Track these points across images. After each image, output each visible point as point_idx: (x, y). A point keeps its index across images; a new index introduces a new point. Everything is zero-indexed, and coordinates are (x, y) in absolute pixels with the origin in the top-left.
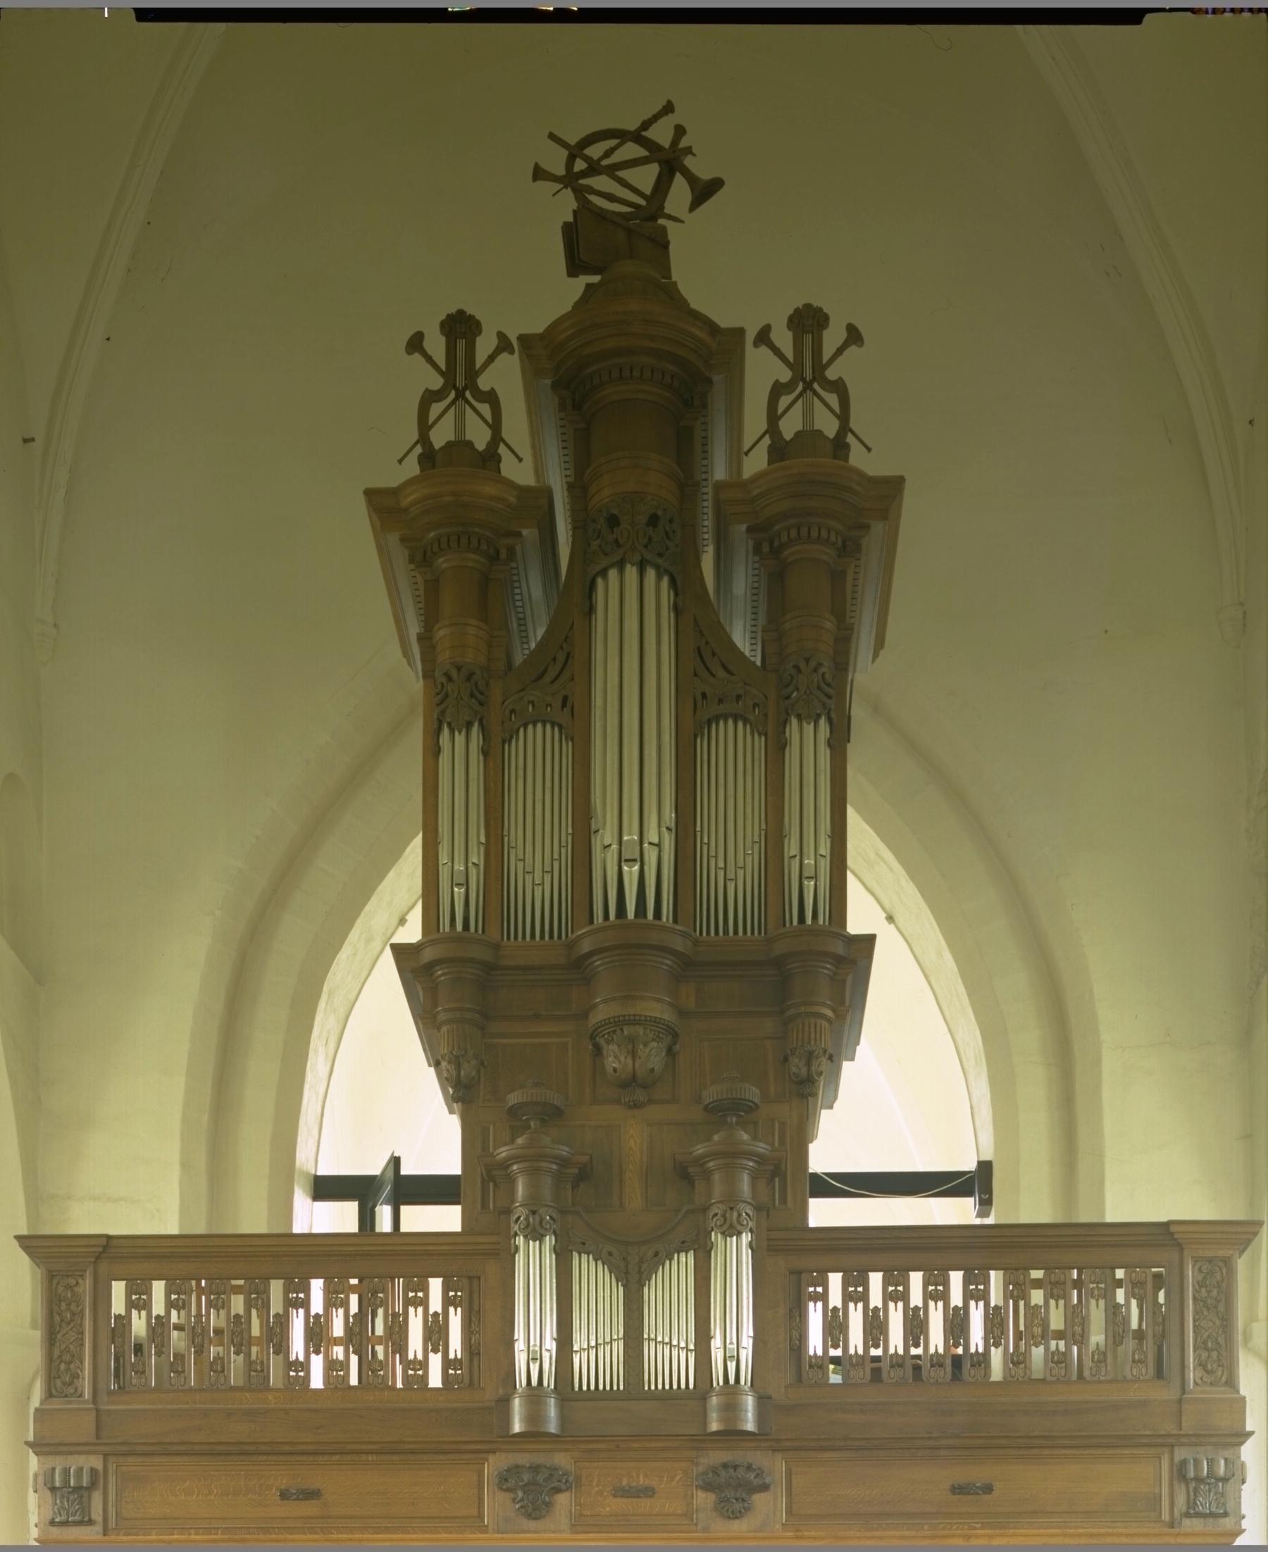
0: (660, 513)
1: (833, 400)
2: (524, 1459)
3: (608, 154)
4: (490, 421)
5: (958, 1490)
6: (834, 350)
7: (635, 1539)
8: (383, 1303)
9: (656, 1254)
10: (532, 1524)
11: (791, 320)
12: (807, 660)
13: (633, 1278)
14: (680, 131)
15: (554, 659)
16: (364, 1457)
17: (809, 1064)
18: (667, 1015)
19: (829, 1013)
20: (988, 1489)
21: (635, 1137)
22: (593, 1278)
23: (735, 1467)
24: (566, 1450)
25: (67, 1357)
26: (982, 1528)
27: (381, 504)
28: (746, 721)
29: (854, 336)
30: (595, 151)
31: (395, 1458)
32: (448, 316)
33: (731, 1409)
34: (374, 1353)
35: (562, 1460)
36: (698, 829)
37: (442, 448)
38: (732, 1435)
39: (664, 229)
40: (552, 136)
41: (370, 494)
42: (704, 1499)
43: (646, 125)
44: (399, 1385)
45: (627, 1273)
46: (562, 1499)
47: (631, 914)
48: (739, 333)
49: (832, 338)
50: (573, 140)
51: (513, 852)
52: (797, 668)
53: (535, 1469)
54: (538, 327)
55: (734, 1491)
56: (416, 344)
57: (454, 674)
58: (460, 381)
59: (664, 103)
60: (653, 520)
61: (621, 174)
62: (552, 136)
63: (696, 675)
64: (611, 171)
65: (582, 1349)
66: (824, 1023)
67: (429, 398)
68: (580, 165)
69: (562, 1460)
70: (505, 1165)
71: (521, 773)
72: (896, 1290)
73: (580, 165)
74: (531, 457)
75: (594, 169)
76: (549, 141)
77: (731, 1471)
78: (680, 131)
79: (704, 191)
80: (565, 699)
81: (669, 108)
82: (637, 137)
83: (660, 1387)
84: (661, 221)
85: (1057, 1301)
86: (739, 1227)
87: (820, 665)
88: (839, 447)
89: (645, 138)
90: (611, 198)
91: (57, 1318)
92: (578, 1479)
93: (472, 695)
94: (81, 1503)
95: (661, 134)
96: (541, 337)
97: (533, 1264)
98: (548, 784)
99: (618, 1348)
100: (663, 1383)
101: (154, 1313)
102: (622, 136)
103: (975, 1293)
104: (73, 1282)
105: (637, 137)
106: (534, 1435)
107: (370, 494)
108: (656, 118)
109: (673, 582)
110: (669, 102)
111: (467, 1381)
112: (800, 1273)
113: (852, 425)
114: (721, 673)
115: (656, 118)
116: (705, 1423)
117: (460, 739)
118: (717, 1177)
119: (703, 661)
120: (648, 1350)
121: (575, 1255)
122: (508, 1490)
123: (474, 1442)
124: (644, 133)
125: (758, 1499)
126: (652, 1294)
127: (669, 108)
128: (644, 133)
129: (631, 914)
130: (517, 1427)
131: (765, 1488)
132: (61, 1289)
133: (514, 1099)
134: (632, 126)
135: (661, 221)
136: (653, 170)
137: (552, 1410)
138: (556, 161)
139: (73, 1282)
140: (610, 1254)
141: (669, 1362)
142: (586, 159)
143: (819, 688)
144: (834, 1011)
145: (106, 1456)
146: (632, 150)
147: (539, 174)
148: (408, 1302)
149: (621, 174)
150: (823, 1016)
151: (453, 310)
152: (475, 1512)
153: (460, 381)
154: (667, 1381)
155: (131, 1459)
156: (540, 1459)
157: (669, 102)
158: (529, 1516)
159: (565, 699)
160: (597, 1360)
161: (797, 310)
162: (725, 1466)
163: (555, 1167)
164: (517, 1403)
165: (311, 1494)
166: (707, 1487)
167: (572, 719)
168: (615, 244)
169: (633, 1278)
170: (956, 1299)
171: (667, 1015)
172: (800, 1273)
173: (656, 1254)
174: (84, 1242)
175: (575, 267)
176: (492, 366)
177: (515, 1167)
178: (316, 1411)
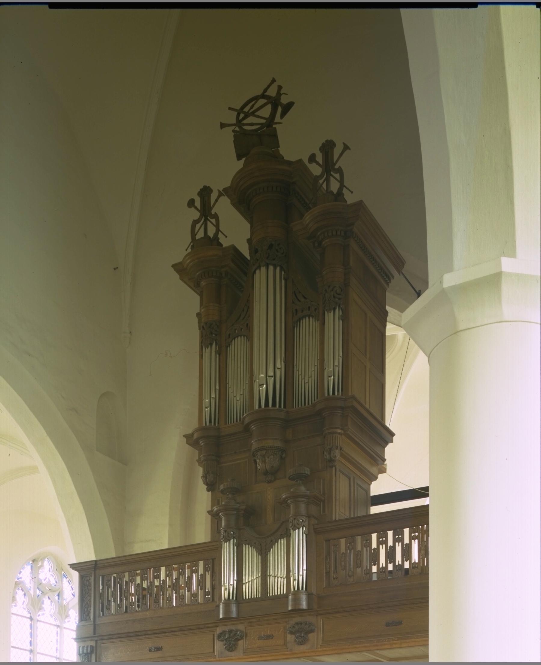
0: (273, 243)
1: (213, 221)
2: (227, 628)
3: (252, 108)
4: (215, 224)
5: (388, 625)
6: (339, 155)
7: (266, 656)
8: (147, 579)
9: (272, 541)
10: (232, 654)
11: (320, 149)
12: (329, 287)
13: (263, 554)
14: (280, 88)
15: (243, 310)
16: (176, 633)
17: (330, 454)
18: (278, 444)
19: (339, 431)
20: (400, 623)
21: (268, 494)
22: (251, 555)
23: (301, 624)
24: (242, 623)
25: (87, 606)
26: (398, 640)
27: (178, 268)
28: (313, 317)
29: (346, 148)
30: (246, 109)
31: (186, 632)
32: (201, 189)
33: (297, 600)
34: (132, 599)
35: (241, 627)
36: (295, 365)
37: (199, 239)
38: (297, 611)
39: (275, 129)
40: (230, 109)
41: (174, 266)
42: (290, 638)
43: (265, 90)
44: (174, 605)
45: (261, 550)
46: (241, 643)
47: (263, 406)
48: (300, 161)
49: (337, 152)
50: (238, 108)
51: (230, 389)
52: (326, 290)
53: (230, 631)
54: (228, 184)
55: (302, 633)
56: (191, 203)
57: (205, 326)
58: (206, 212)
59: (272, 79)
60: (271, 247)
61: (256, 114)
62: (230, 109)
63: (293, 303)
64: (253, 114)
65: (249, 581)
66: (339, 436)
67: (195, 222)
68: (242, 116)
69: (241, 627)
70: (285, 501)
71: (233, 358)
72: (415, 535)
73: (242, 116)
74: (235, 231)
75: (247, 116)
76: (230, 111)
77: (299, 625)
78: (280, 88)
79: (287, 108)
80: (247, 324)
81: (274, 81)
82: (263, 96)
83: (279, 593)
84: (274, 126)
85: (367, 548)
86: (298, 526)
87: (335, 287)
88: (340, 194)
89: (266, 95)
90: (252, 124)
91: (84, 592)
92: (246, 635)
93: (334, 297)
94: (88, 659)
95: (272, 92)
96: (230, 187)
97: (228, 551)
98: (242, 360)
99: (259, 581)
100: (274, 593)
101: (162, 579)
102: (256, 99)
103: (398, 539)
104: (88, 578)
105: (263, 96)
106: (227, 619)
107: (174, 266)
108: (269, 86)
109: (282, 269)
110: (273, 78)
111: (211, 599)
112: (329, 540)
113: (345, 184)
114: (303, 300)
115: (269, 86)
116: (288, 607)
117: (208, 350)
118: (292, 506)
119: (296, 296)
120: (269, 580)
121: (244, 546)
122: (221, 641)
123: (212, 623)
124: (265, 94)
125: (310, 636)
126: (271, 557)
127: (274, 81)
128: (265, 94)
129: (263, 406)
130: (221, 617)
131: (312, 631)
132: (85, 582)
133: (222, 487)
134: (260, 93)
135: (274, 126)
136: (269, 107)
137: (234, 608)
138: (232, 118)
139: (88, 578)
140: (255, 543)
141: (277, 584)
142: (244, 113)
143: (334, 297)
144: (342, 429)
145: (96, 641)
146: (262, 102)
147: (223, 126)
148: (192, 572)
149: (256, 114)
150: (336, 433)
151: (202, 187)
152: (212, 650)
153: (206, 212)
154: (279, 590)
155: (104, 641)
156: (233, 628)
157: (273, 78)
158: (228, 650)
159: (247, 324)
160: (251, 586)
161: (323, 144)
162: (297, 624)
163: (235, 512)
164: (221, 606)
165: (158, 649)
166: (291, 633)
167: (247, 331)
168: (255, 141)
169: (263, 554)
170: (390, 543)
171: (279, 444)
172: (329, 540)
173: (272, 541)
174: (144, 555)
175: (239, 158)
176: (342, 158)
177: (289, 501)
178: (161, 617)
